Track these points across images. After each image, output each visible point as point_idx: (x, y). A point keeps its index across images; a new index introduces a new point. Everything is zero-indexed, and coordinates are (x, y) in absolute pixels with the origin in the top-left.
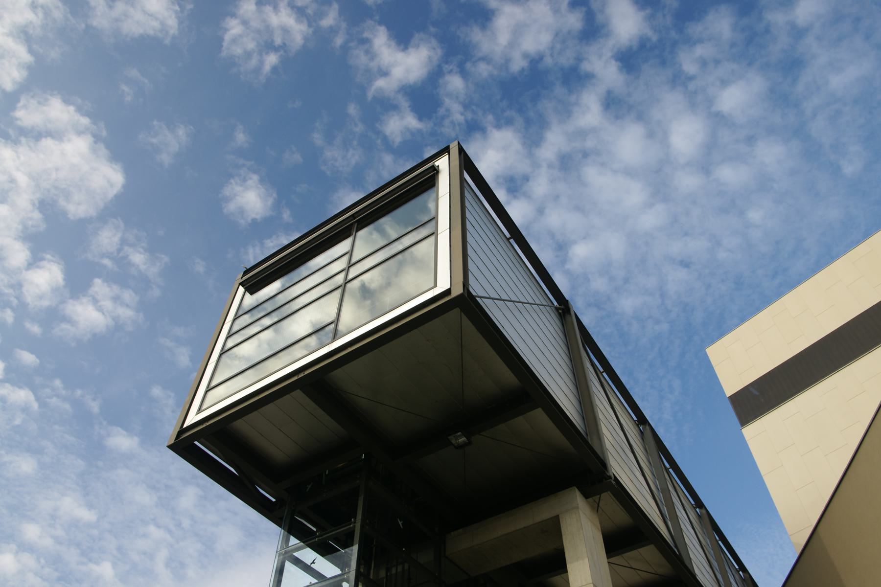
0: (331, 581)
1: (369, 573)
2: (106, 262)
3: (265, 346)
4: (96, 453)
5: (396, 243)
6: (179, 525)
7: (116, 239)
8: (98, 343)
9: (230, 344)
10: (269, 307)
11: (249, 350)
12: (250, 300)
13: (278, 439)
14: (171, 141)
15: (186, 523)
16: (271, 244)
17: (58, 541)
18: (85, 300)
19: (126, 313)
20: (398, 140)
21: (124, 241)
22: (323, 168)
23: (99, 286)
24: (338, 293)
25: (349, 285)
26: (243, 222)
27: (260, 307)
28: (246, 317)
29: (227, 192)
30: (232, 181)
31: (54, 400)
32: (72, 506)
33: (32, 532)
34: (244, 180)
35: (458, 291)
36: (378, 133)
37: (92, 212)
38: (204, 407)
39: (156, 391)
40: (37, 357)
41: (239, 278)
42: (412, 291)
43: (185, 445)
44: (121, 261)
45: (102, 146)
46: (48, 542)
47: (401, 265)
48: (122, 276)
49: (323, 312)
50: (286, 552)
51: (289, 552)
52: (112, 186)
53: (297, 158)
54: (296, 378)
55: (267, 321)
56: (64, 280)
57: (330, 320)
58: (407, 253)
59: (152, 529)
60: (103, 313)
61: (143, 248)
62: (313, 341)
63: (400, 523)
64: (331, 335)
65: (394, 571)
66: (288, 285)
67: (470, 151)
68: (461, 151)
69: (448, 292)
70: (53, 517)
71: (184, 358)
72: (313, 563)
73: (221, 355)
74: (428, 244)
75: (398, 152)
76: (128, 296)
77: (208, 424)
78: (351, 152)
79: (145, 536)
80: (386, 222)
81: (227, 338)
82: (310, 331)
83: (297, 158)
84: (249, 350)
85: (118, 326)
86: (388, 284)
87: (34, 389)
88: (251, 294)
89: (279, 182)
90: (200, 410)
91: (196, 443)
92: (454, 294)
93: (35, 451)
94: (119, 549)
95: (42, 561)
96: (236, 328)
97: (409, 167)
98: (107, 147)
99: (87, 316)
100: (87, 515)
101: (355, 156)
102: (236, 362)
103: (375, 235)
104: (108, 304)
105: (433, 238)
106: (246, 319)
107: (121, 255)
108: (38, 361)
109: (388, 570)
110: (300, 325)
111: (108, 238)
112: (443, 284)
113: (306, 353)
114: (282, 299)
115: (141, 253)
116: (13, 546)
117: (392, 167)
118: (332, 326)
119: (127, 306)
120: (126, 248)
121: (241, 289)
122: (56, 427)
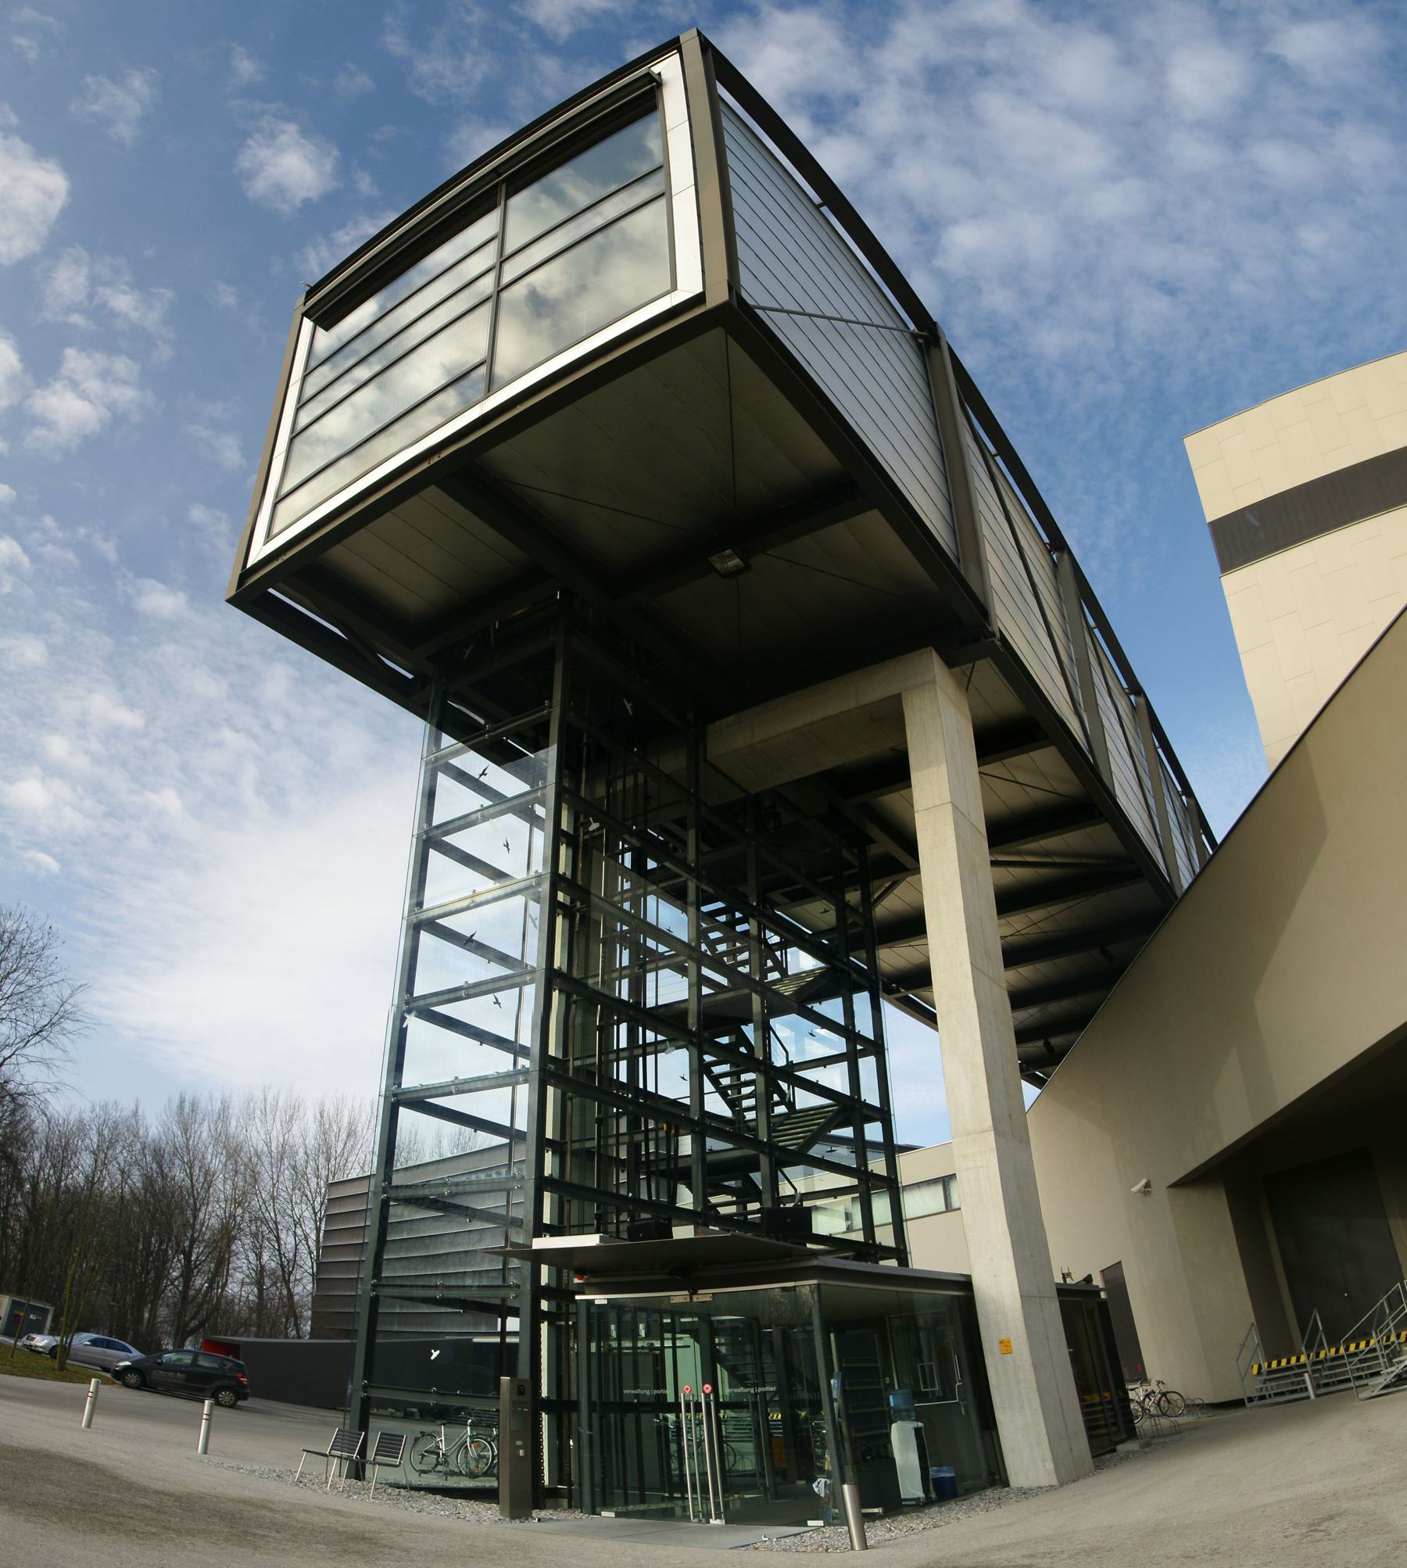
0: (516, 802)
1: (578, 789)
2: (76, 319)
3: (366, 416)
4: (124, 621)
5: (589, 215)
6: (267, 726)
7: (82, 279)
8: (96, 449)
9: (304, 419)
10: (362, 347)
11: (340, 426)
12: (326, 340)
13: (409, 571)
14: (125, 101)
15: (278, 723)
16: (347, 239)
17: (97, 760)
18: (58, 386)
19: (126, 395)
20: (565, 31)
21: (94, 281)
22: (419, 93)
23: (75, 360)
24: (486, 310)
25: (505, 295)
26: (286, 208)
27: (346, 350)
28: (324, 369)
29: (245, 162)
30: (251, 142)
31: (49, 549)
32: (105, 706)
33: (57, 746)
34: (272, 136)
35: (719, 296)
36: (520, 21)
37: (35, 247)
38: (275, 530)
39: (198, 514)
40: (12, 487)
41: (299, 304)
42: (629, 297)
43: (254, 595)
44: (100, 313)
45: (17, 140)
46: (81, 762)
47: (603, 253)
48: (106, 336)
49: (465, 345)
50: (437, 759)
51: (442, 757)
52: (51, 196)
53: (363, 82)
54: (425, 466)
55: (363, 373)
56: (21, 361)
57: (478, 360)
58: (612, 232)
59: (227, 734)
60: (91, 402)
61: (127, 283)
62: (450, 398)
63: (629, 706)
64: (483, 386)
65: (619, 786)
66: (390, 306)
67: (728, 46)
68: (706, 46)
69: (699, 299)
70: (82, 724)
71: (231, 453)
72: (484, 774)
73: (291, 440)
74: (649, 220)
75: (569, 52)
76: (122, 366)
77: (285, 558)
78: (469, 60)
79: (219, 745)
80: (561, 176)
81: (298, 410)
82: (443, 381)
83: (363, 82)
84: (340, 426)
85: (117, 418)
86: (582, 288)
87: (18, 537)
88: (327, 329)
89: (341, 131)
90: (269, 537)
91: (271, 590)
92: (712, 302)
93: (40, 629)
94: (184, 768)
95: (79, 789)
96: (309, 391)
97: (596, 76)
98: (25, 139)
99: (70, 408)
100: (130, 719)
101: (479, 67)
102: (321, 449)
103: (546, 203)
104: (94, 386)
105: (662, 202)
106: (325, 374)
107: (95, 302)
108: (14, 493)
109: (610, 784)
110: (424, 372)
111: (68, 281)
112: (690, 285)
113: (439, 420)
114: (383, 330)
115: (126, 293)
116: (37, 770)
117: (556, 81)
118: (483, 370)
119: (125, 382)
120: (101, 290)
121: (308, 324)
122: (61, 590)
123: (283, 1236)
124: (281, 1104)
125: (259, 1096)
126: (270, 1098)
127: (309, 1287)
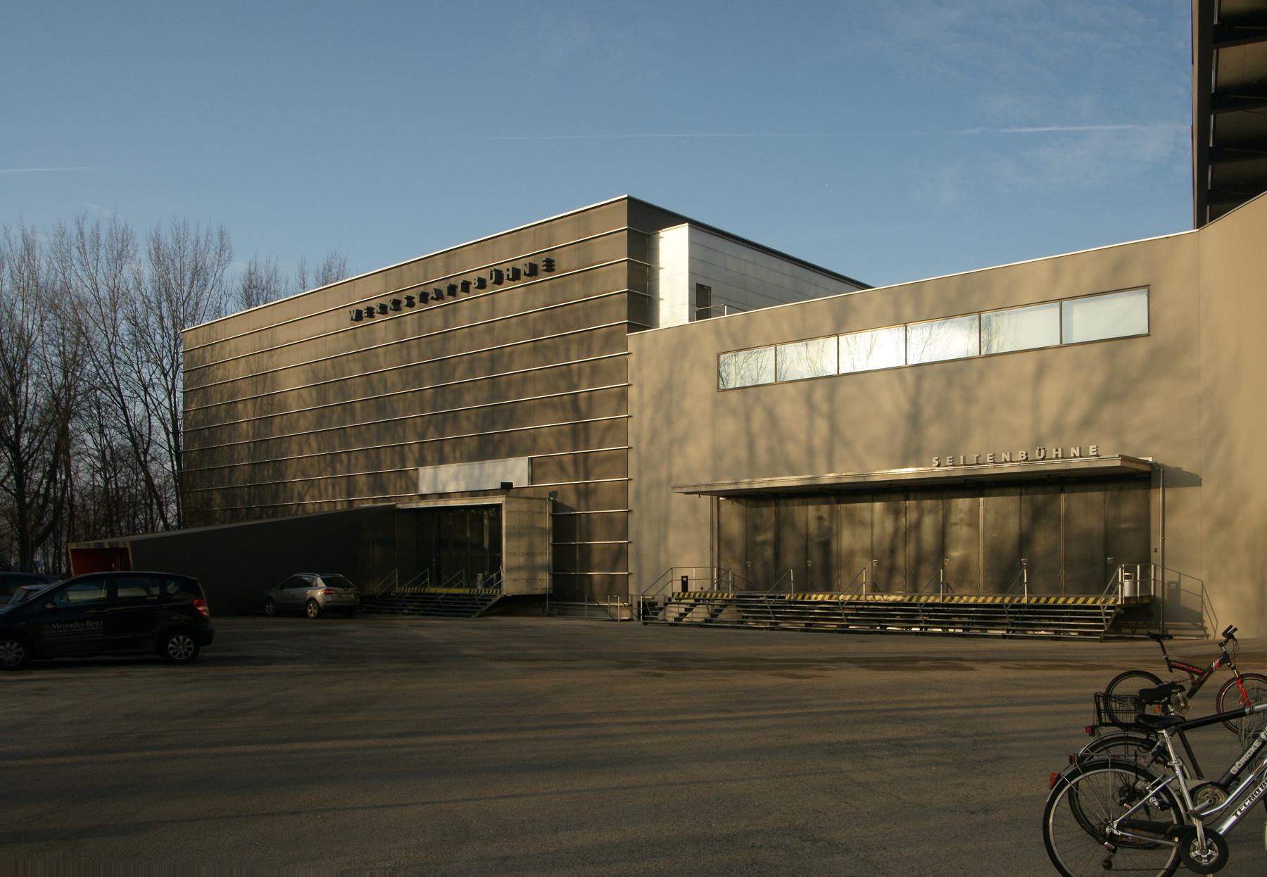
123: (130, 406)
124: (103, 238)
125: (73, 230)
126: (87, 232)
127: (168, 466)
